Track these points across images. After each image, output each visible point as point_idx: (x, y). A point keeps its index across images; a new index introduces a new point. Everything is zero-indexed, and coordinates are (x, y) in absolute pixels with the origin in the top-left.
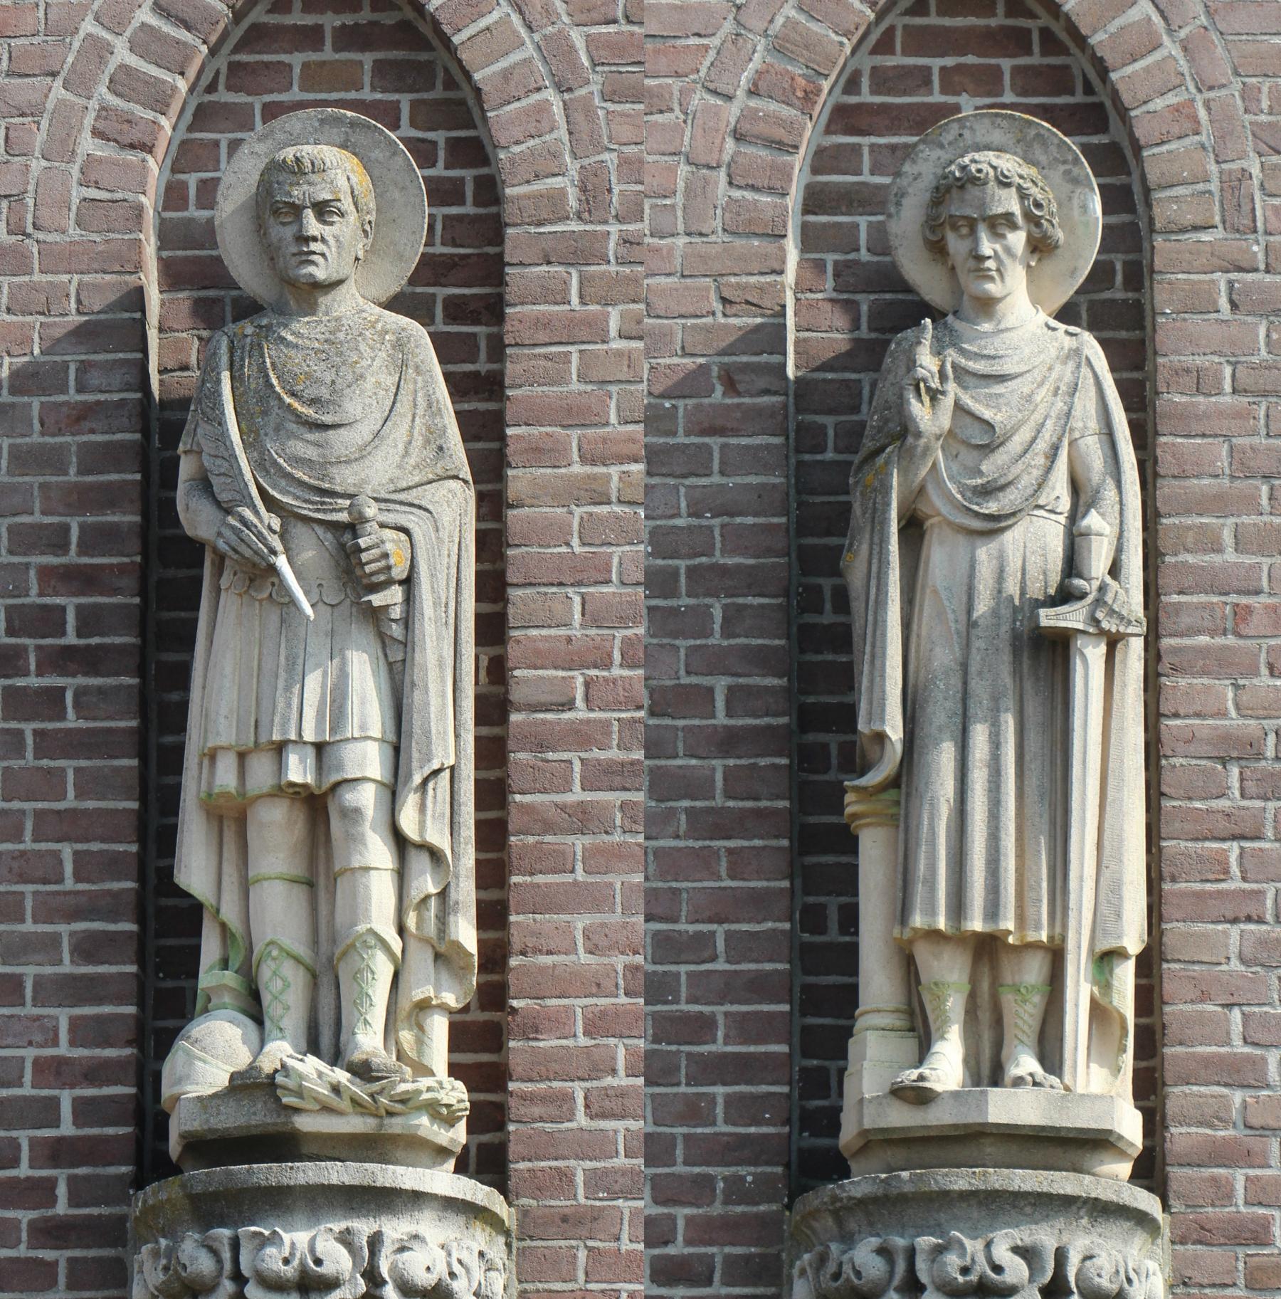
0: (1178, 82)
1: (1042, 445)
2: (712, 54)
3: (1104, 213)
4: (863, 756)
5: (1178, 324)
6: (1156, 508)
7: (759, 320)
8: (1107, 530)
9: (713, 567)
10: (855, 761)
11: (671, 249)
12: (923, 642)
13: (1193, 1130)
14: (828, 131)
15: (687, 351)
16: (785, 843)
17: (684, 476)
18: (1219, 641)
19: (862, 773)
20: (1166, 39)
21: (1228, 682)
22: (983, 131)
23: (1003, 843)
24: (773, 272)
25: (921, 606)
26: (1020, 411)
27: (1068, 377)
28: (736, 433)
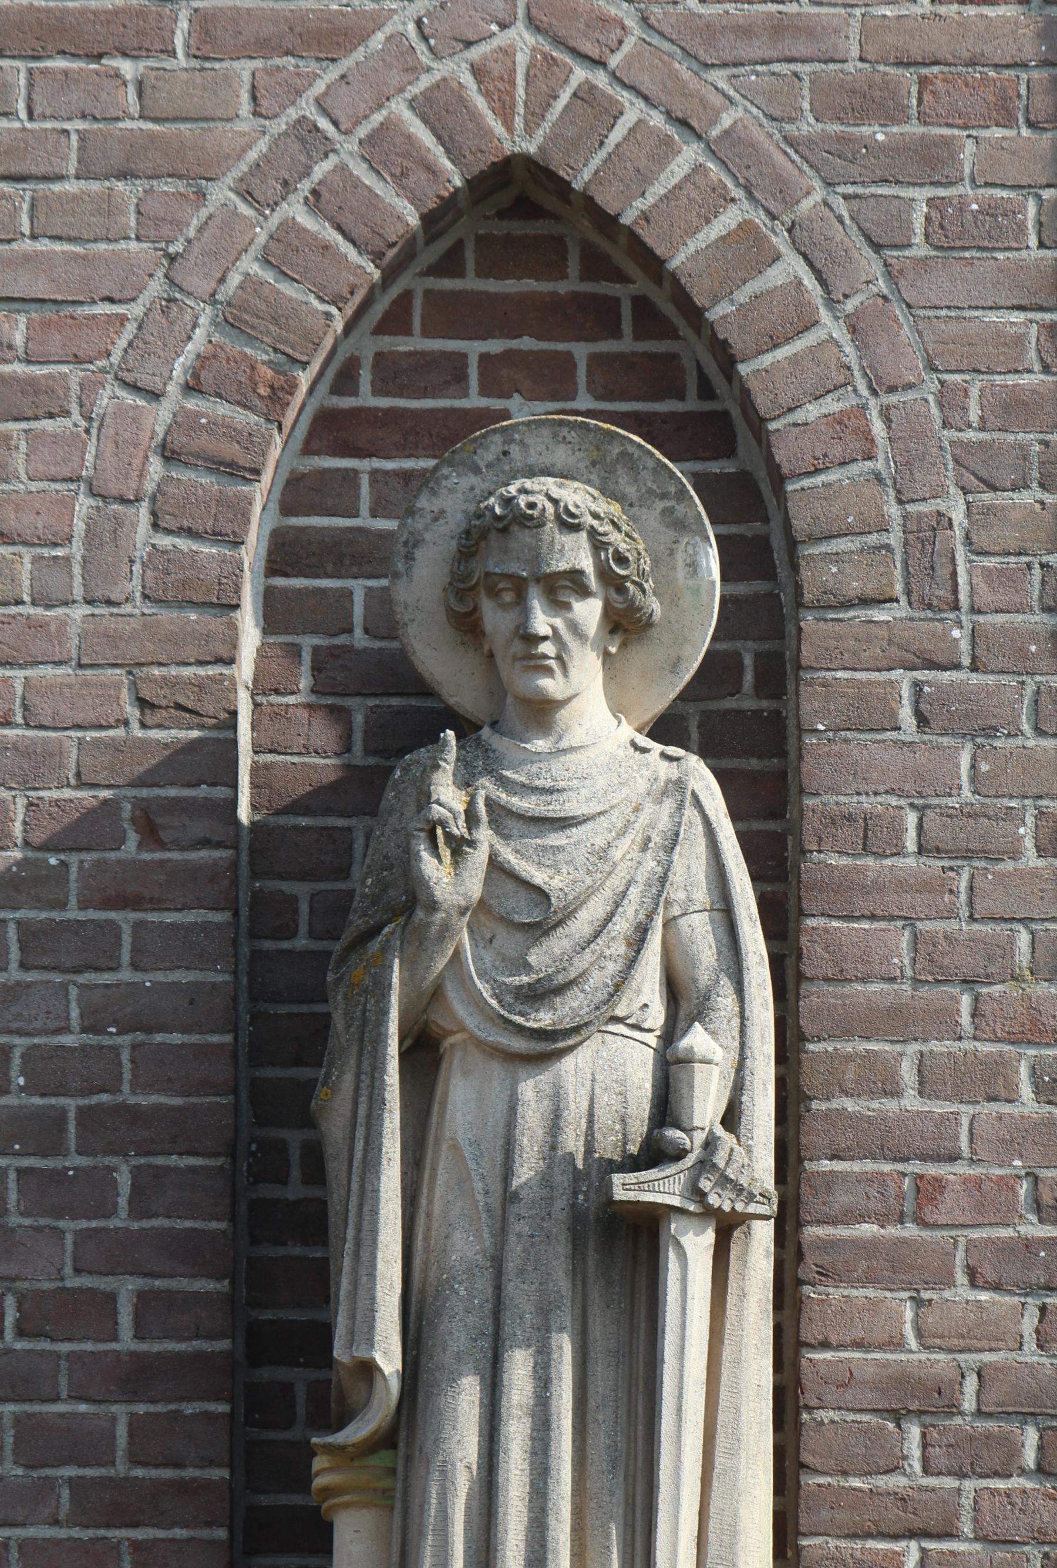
0: (842, 379)
1: (622, 925)
2: (131, 328)
3: (724, 578)
4: (342, 1399)
5: (836, 748)
6: (799, 1027)
7: (195, 734)
8: (719, 1055)
9: (120, 1110)
10: (332, 1410)
11: (63, 624)
12: (435, 1225)
14: (308, 449)
15: (85, 779)
16: (222, 1534)
17: (77, 970)
18: (893, 1231)
19: (341, 1425)
21: (905, 1295)
22: (539, 447)
23: (551, 1534)
25: (434, 1169)
26: (589, 872)
27: (664, 823)
28: (157, 905)
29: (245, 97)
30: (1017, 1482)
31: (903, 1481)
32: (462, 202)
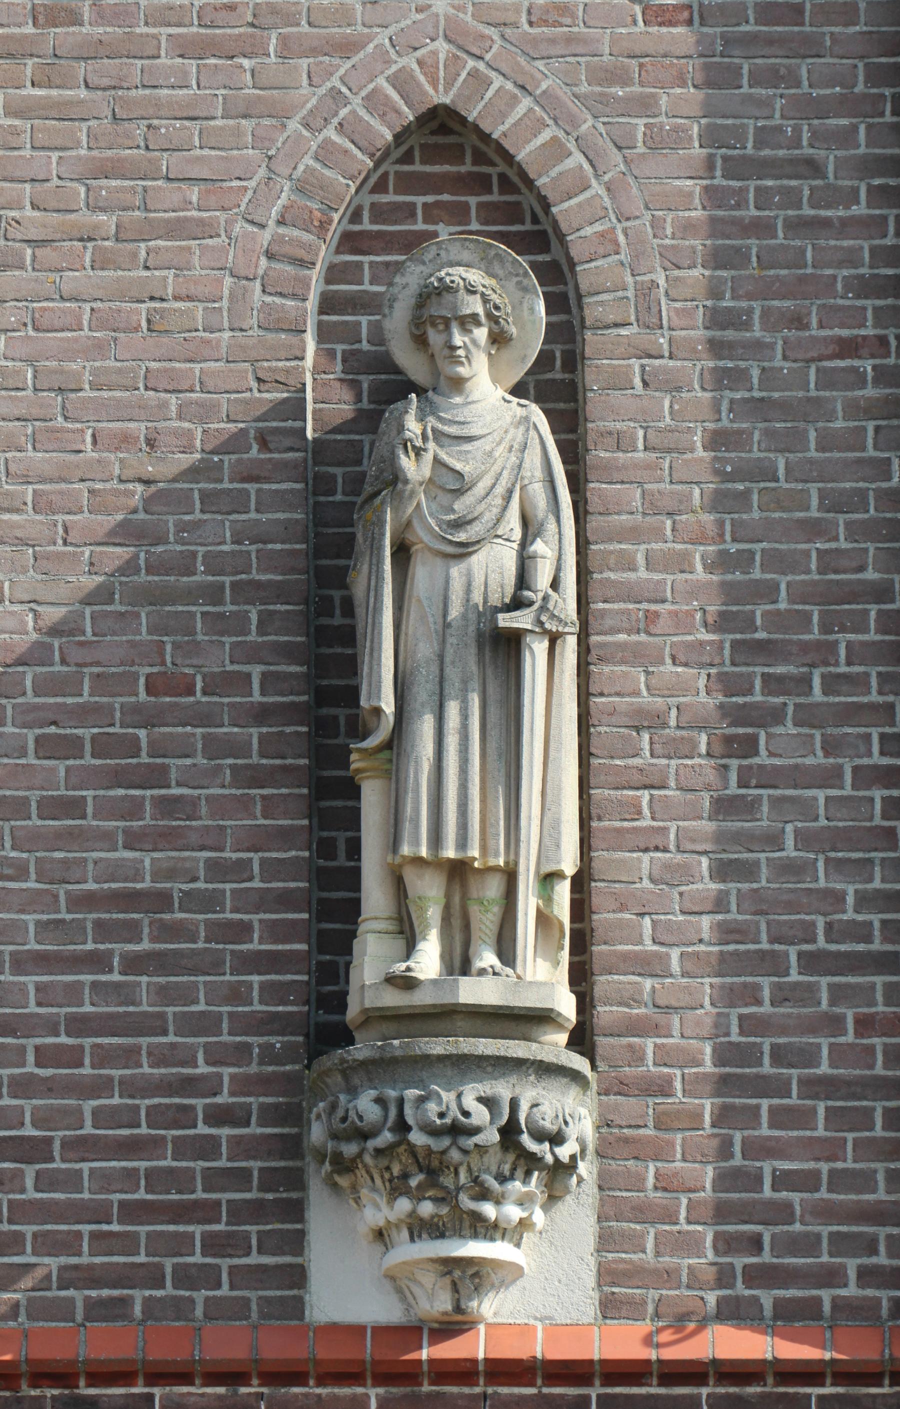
1: (500, 490)
2: (250, 193)
4: (365, 725)
7: (285, 395)
9: (251, 582)
11: (219, 341)
13: (615, 1008)
14: (338, 251)
17: (229, 513)
18: (634, 638)
19: (364, 738)
20: (594, 182)
22: (455, 252)
24: (296, 358)
27: (520, 438)
28: (268, 480)
29: (305, 76)
30: (697, 761)
31: (641, 761)
32: (413, 127)
